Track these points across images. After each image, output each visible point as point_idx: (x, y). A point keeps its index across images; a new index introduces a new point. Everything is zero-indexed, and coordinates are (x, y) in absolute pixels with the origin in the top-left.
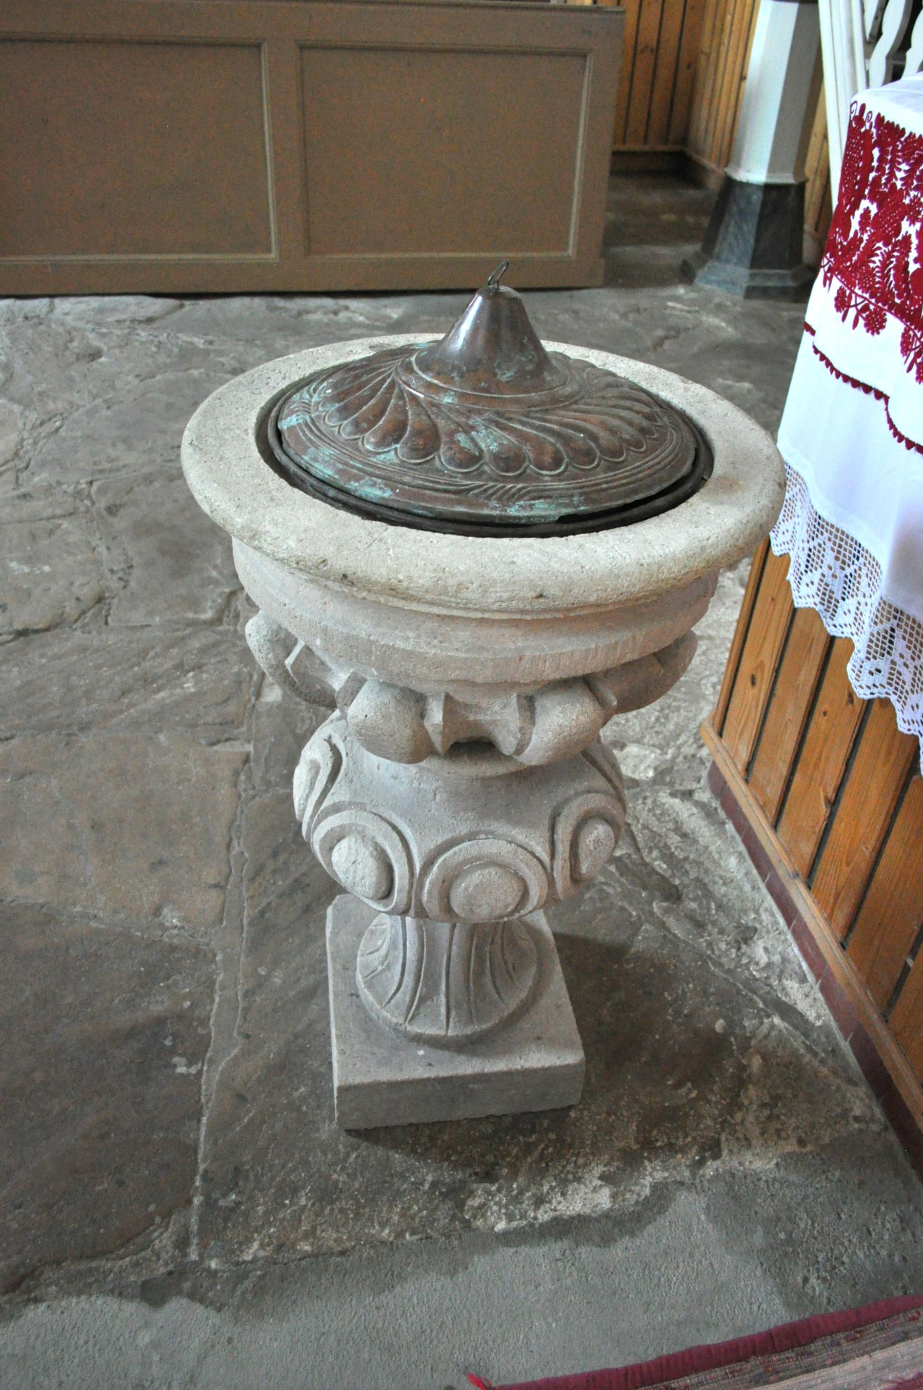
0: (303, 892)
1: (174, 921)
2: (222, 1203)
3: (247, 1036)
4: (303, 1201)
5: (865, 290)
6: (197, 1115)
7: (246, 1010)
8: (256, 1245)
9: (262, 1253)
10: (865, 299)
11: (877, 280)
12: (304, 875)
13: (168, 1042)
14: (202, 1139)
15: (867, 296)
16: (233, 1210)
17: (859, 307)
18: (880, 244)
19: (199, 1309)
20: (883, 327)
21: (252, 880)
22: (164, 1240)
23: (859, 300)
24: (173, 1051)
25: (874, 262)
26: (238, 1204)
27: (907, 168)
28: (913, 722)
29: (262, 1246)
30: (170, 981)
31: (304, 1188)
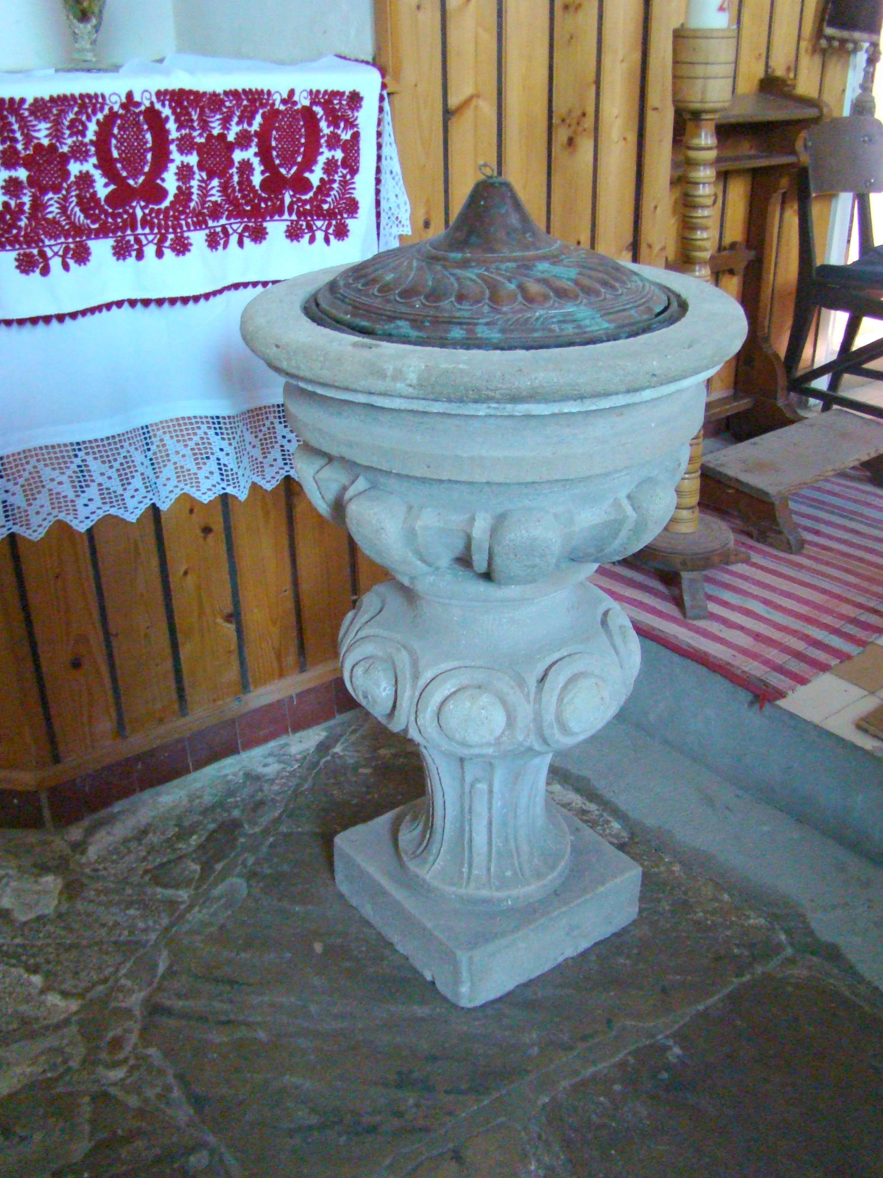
0: (410, 1072)
1: (533, 1168)
2: (746, 953)
3: (609, 1021)
4: (701, 914)
5: (56, 237)
6: (704, 1014)
7: (584, 1038)
8: (752, 921)
9: (752, 914)
10: (62, 243)
11: (64, 223)
12: (385, 1085)
13: (664, 1075)
14: (716, 998)
15: (63, 240)
16: (744, 946)
17: (61, 253)
18: (50, 195)
19: (813, 924)
20: (89, 254)
21: (426, 1130)
22: (799, 972)
23: (56, 249)
24: (667, 1067)
25: (51, 212)
26: (738, 946)
27: (49, 125)
28: (214, 486)
29: (748, 917)
30: (605, 1120)
31: (692, 920)
